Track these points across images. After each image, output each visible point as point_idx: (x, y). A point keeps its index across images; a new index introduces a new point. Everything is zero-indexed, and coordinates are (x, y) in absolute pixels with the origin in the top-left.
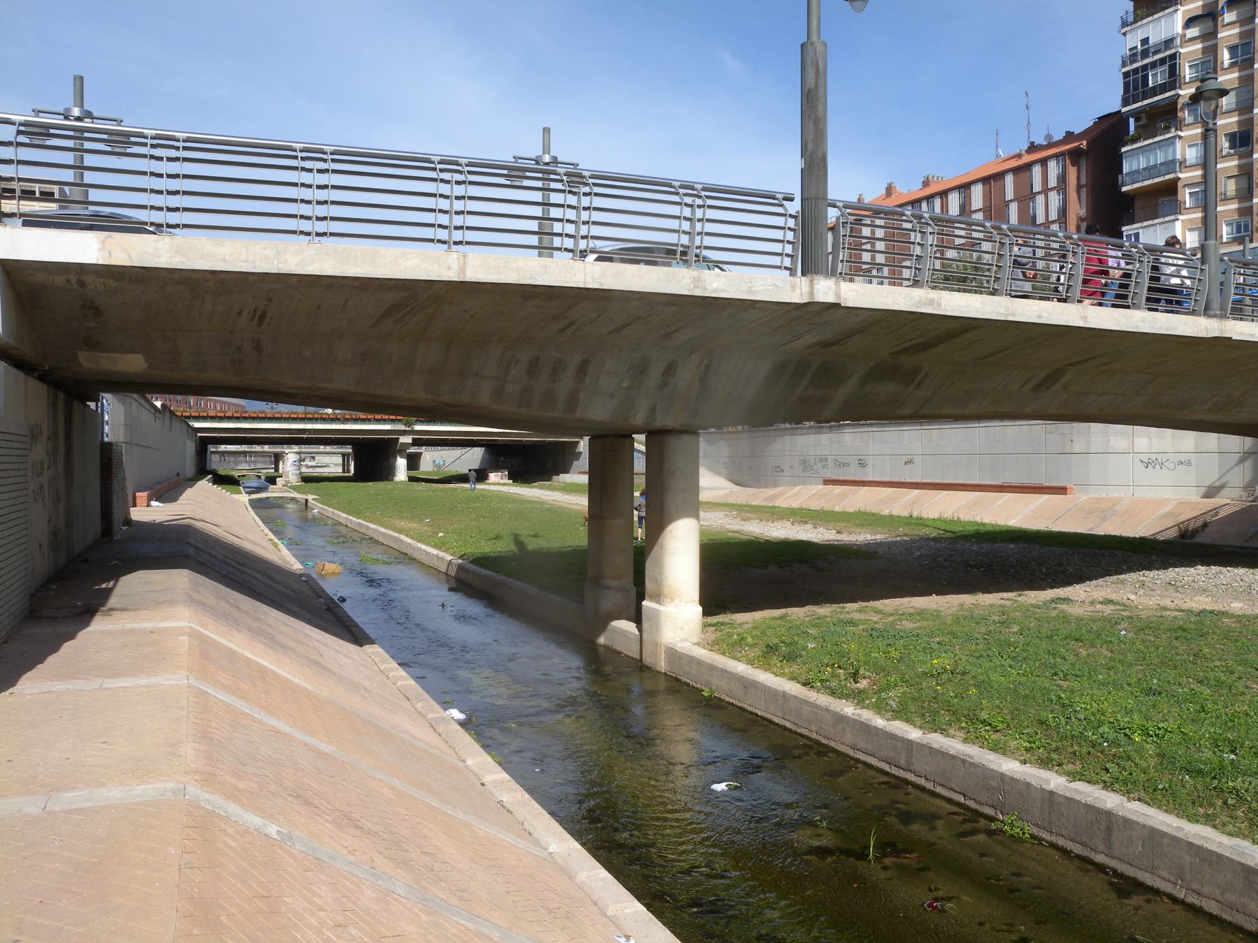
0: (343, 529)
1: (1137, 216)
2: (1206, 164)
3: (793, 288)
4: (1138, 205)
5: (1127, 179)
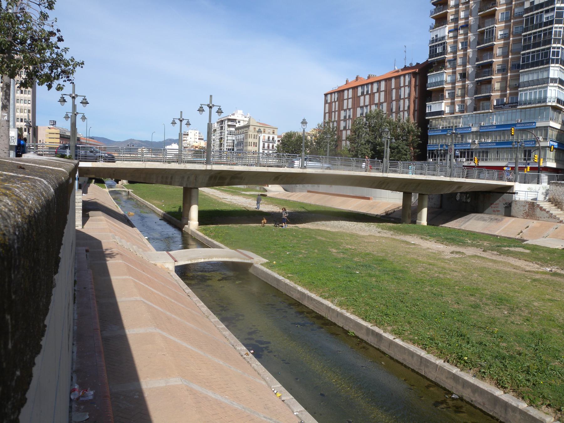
0: (139, 202)
1: (432, 100)
2: (453, 83)
3: (203, 167)
4: (433, 95)
5: (429, 85)
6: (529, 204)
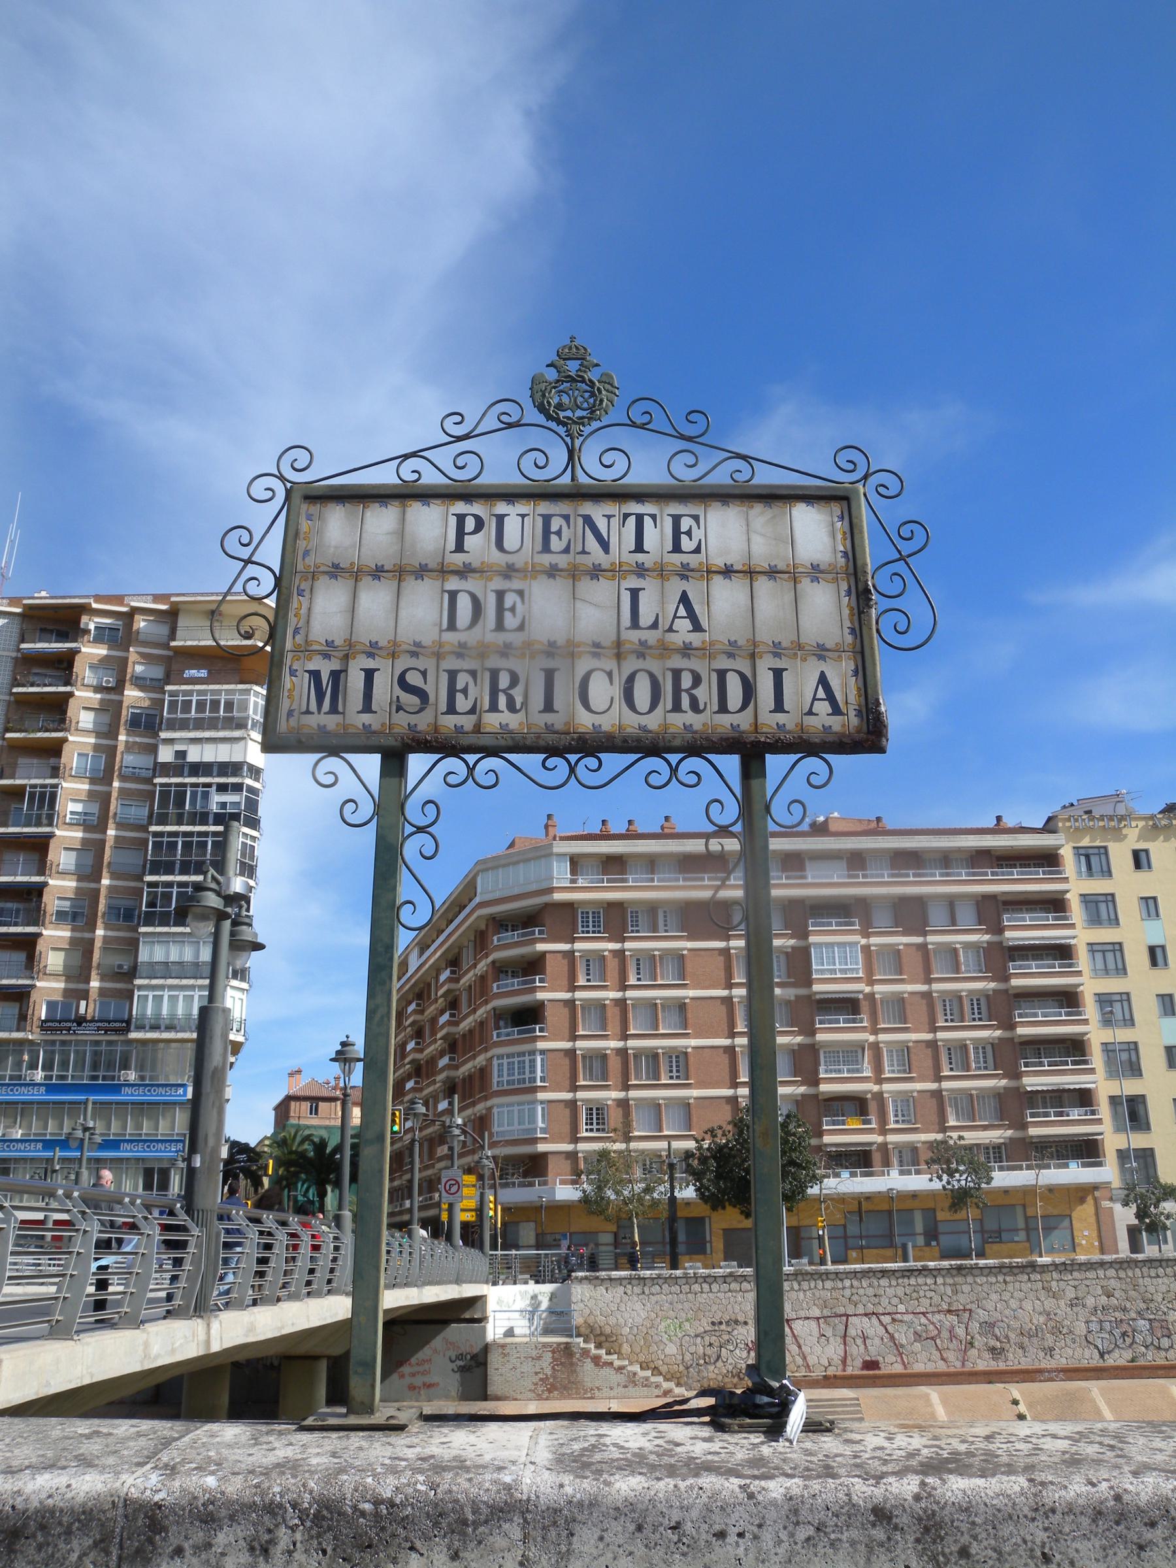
6: (553, 1352)
